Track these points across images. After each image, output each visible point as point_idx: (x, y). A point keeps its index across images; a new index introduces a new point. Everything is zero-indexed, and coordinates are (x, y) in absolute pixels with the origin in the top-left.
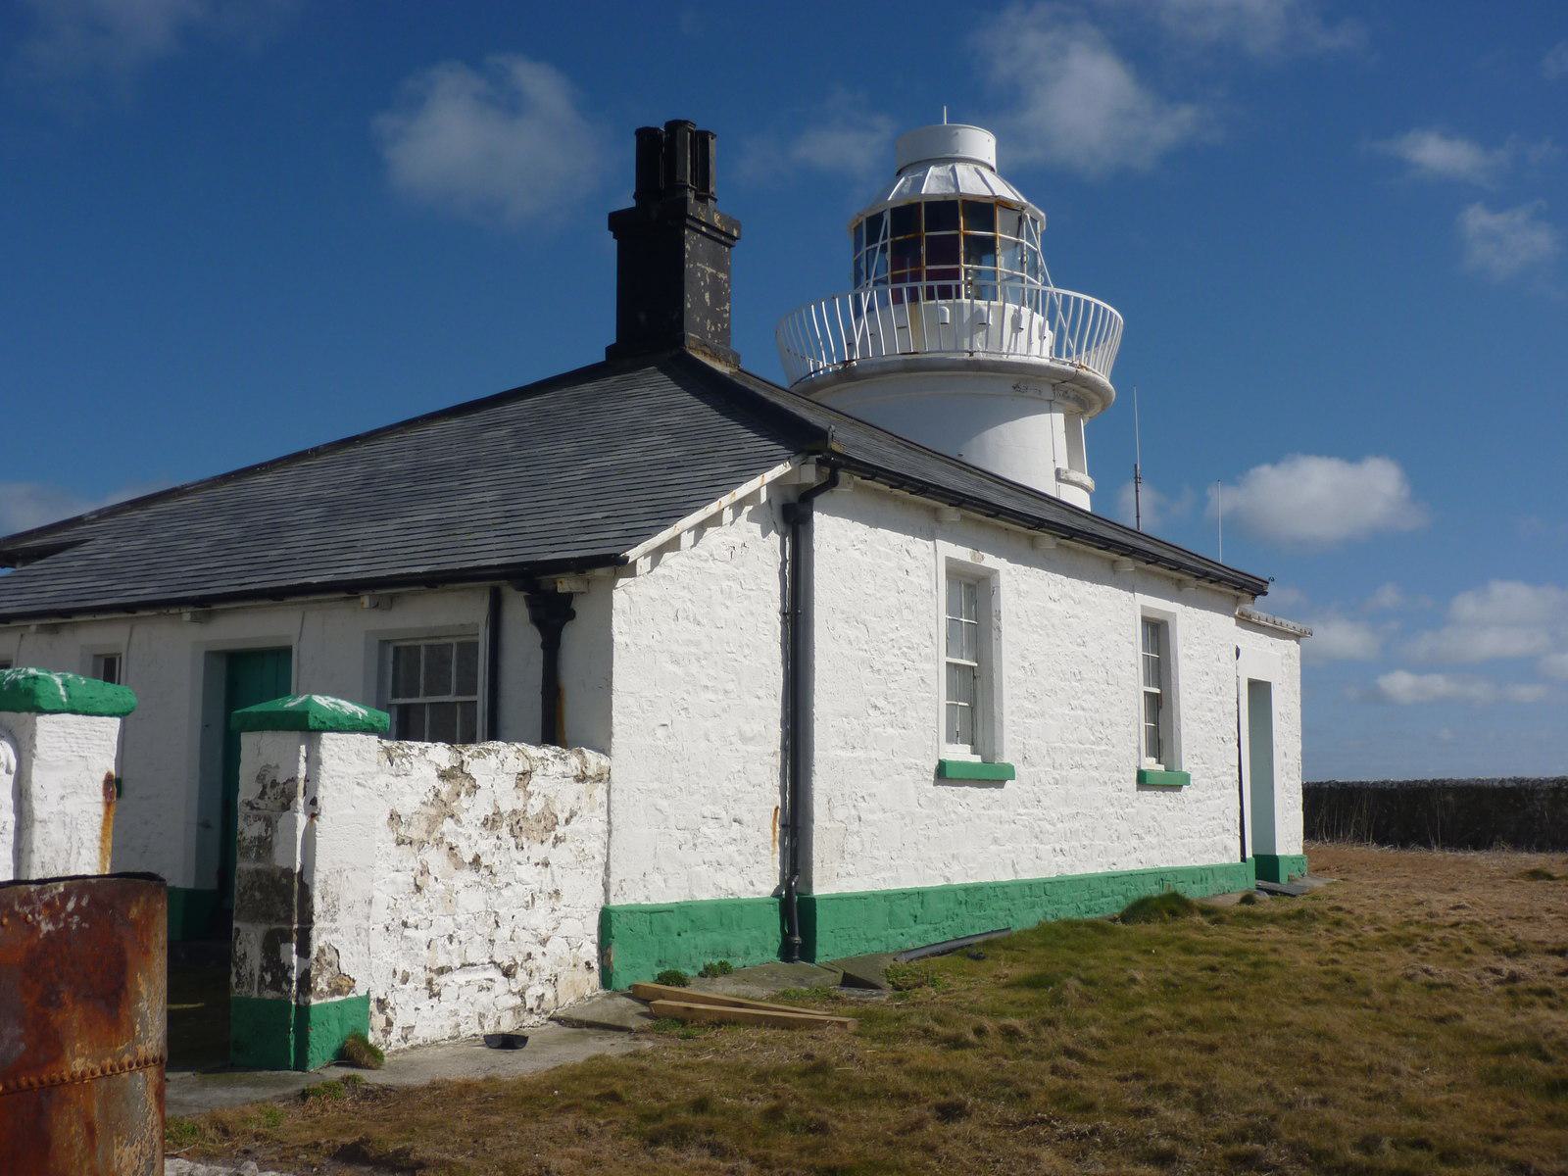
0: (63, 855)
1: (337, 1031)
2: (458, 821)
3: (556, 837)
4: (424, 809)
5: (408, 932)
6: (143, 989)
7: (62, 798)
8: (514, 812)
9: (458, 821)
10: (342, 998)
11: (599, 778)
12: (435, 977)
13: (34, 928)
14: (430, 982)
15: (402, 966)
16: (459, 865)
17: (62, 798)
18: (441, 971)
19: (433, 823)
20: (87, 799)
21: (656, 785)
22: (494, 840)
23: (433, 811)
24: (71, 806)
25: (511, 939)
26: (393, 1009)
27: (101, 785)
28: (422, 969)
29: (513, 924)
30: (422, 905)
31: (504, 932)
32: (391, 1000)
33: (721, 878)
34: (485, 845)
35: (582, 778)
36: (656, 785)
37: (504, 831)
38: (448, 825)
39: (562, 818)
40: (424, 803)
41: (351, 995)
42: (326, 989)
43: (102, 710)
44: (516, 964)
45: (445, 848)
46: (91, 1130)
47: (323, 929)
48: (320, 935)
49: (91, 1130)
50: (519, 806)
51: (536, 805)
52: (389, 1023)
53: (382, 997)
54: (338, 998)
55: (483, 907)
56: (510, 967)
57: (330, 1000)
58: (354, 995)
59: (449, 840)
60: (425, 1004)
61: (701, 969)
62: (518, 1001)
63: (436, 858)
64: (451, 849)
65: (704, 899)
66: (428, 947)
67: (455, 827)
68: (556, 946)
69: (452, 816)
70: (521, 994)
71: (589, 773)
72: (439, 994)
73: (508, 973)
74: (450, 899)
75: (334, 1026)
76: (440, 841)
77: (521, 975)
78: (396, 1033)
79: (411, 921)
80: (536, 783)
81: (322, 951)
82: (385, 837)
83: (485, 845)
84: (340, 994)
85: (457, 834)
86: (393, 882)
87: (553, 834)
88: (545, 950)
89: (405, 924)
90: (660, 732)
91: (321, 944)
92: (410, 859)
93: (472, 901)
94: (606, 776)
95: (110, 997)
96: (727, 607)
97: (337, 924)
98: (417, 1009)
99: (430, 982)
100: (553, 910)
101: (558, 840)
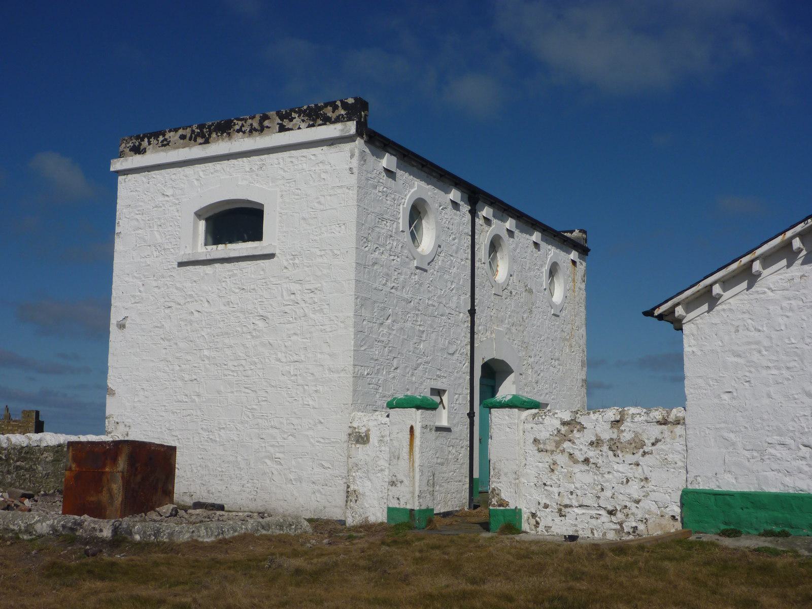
0: (398, 450)
1: (503, 520)
2: (574, 443)
3: (644, 452)
4: (551, 437)
5: (546, 488)
6: (120, 459)
7: (398, 433)
8: (612, 439)
9: (574, 443)
10: (504, 508)
11: (677, 422)
12: (563, 508)
13: (106, 447)
14: (560, 510)
15: (544, 501)
16: (576, 462)
17: (398, 433)
18: (566, 506)
19: (558, 444)
20: (405, 433)
21: (723, 425)
22: (598, 452)
23: (557, 438)
24: (400, 435)
25: (612, 498)
26: (540, 518)
27: (409, 429)
28: (555, 504)
29: (613, 491)
30: (554, 477)
31: (608, 493)
32: (538, 514)
33: (788, 480)
34: (591, 453)
35: (664, 422)
36: (723, 425)
37: (605, 448)
38: (566, 445)
39: (648, 443)
40: (551, 435)
41: (507, 508)
42: (496, 503)
43: (406, 406)
44: (617, 510)
45: (566, 455)
46: (108, 480)
47: (494, 482)
48: (492, 483)
49: (108, 480)
50: (615, 436)
51: (627, 436)
52: (537, 523)
53: (534, 512)
54: (502, 508)
55: (593, 481)
56: (613, 510)
57: (498, 508)
58: (509, 508)
59: (569, 451)
60: (558, 519)
61: (762, 531)
62: (618, 527)
63: (561, 459)
64: (571, 454)
65: (772, 491)
66: (559, 495)
67: (572, 445)
68: (646, 504)
69: (570, 441)
70: (621, 524)
71: (669, 420)
72: (565, 516)
73: (611, 513)
74: (570, 476)
75: (501, 518)
76: (563, 451)
77: (620, 516)
78: (541, 528)
79: (548, 483)
80: (626, 425)
81: (494, 489)
82: (532, 449)
83: (591, 453)
84: (503, 506)
85: (574, 448)
86: (537, 467)
87: (641, 450)
88: (638, 506)
89: (545, 484)
90: (726, 397)
91: (493, 487)
92: (548, 458)
93: (588, 478)
94: (682, 422)
95: (115, 460)
96: (788, 317)
97: (500, 480)
98: (553, 520)
99: (560, 510)
100: (643, 487)
101: (645, 453)
